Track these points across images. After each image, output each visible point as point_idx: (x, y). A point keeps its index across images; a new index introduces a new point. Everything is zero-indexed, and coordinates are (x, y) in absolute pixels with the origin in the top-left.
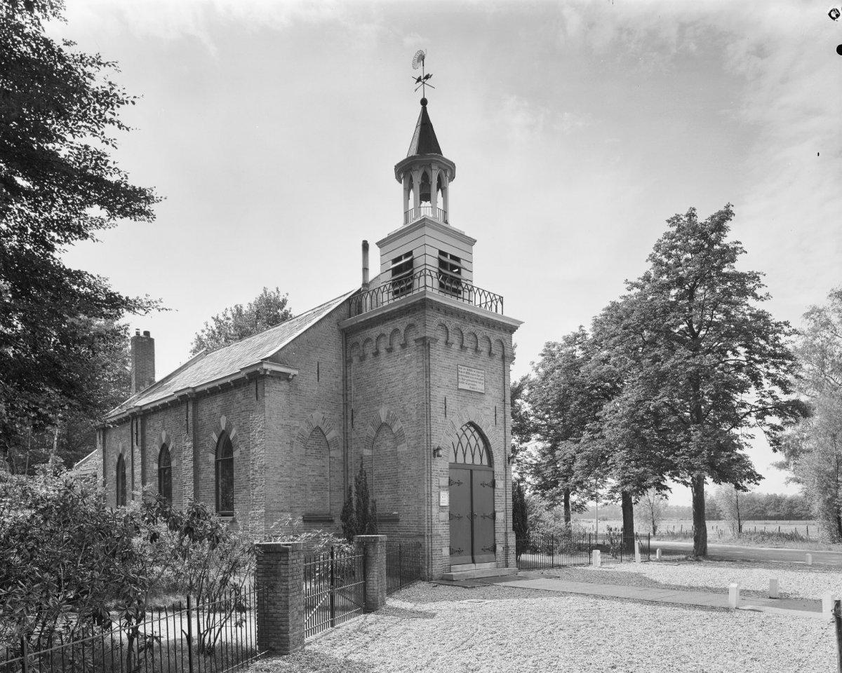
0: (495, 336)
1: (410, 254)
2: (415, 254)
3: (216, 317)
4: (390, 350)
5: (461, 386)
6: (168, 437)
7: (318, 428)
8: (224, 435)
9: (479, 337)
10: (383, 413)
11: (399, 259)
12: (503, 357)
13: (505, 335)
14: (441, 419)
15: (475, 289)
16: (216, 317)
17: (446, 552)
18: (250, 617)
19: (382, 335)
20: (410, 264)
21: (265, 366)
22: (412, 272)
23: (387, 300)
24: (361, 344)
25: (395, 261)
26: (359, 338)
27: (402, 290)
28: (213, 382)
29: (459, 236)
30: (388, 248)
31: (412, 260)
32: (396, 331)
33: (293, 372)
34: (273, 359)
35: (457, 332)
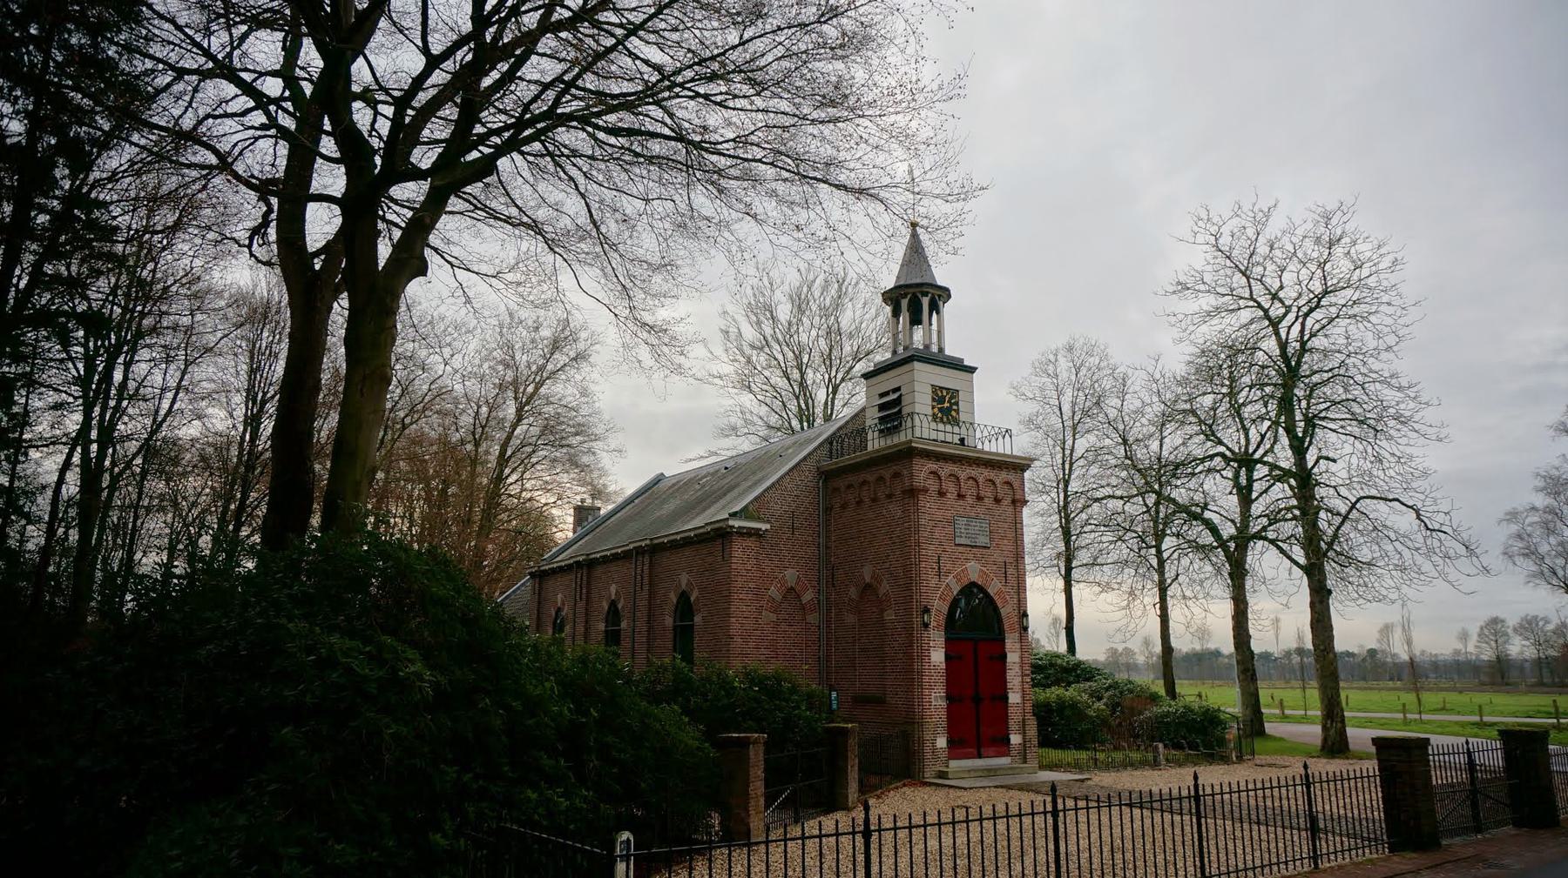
0: (1003, 476)
1: (898, 389)
2: (903, 391)
3: (1240, 255)
4: (874, 500)
5: (958, 541)
6: (689, 583)
7: (792, 588)
8: (684, 597)
9: (981, 480)
10: (867, 574)
11: (886, 394)
12: (1014, 502)
13: (1011, 477)
14: (934, 581)
15: (982, 427)
16: (1240, 255)
17: (942, 742)
18: (1371, 801)
19: (864, 483)
20: (898, 401)
21: (731, 523)
22: (900, 411)
23: (875, 443)
24: (843, 489)
25: (882, 395)
26: (841, 483)
27: (888, 429)
28: (718, 521)
29: (957, 365)
30: (874, 380)
31: (901, 395)
32: (881, 478)
33: (764, 527)
34: (743, 513)
35: (953, 479)
